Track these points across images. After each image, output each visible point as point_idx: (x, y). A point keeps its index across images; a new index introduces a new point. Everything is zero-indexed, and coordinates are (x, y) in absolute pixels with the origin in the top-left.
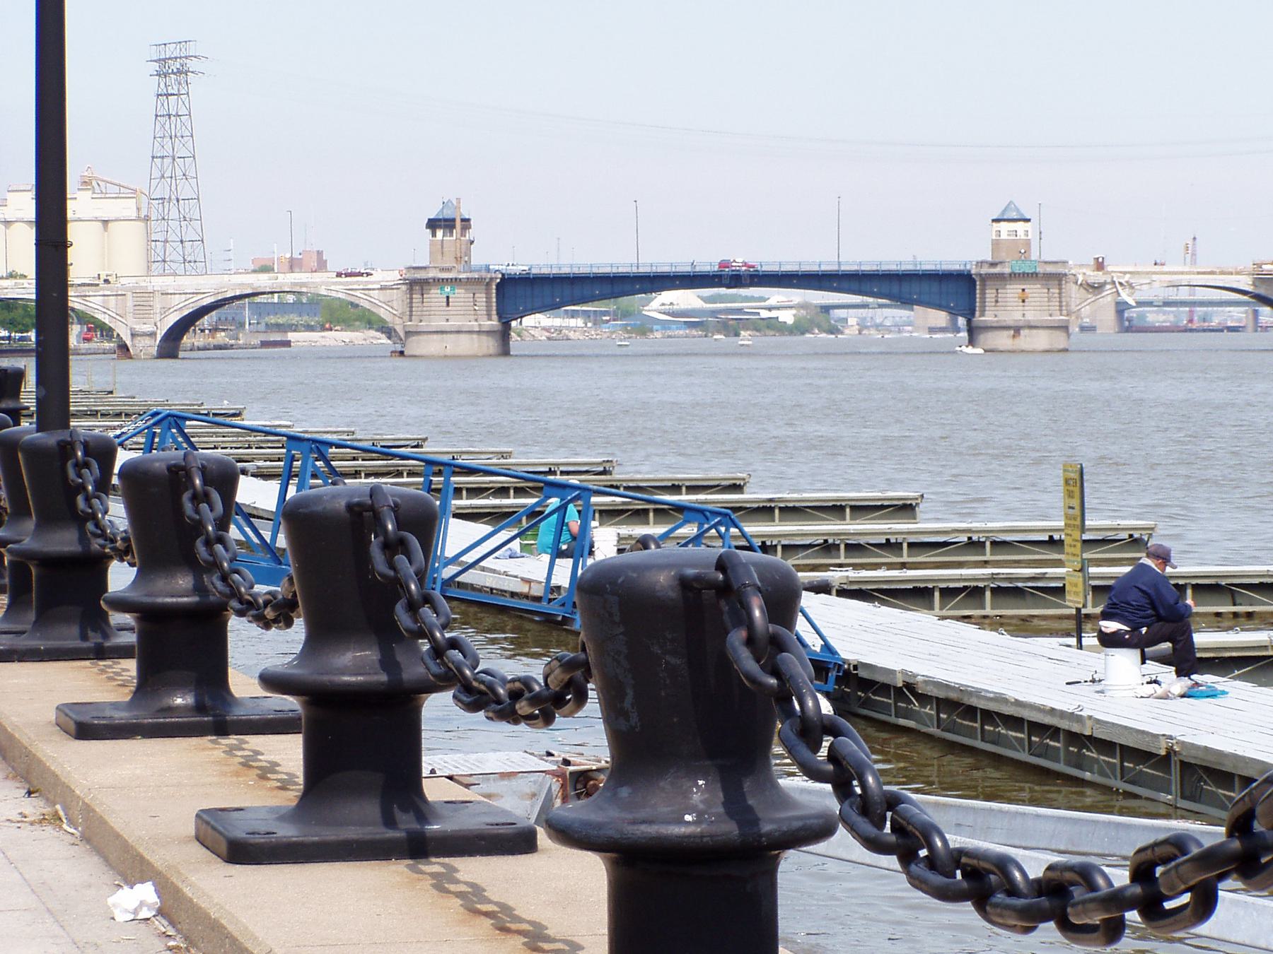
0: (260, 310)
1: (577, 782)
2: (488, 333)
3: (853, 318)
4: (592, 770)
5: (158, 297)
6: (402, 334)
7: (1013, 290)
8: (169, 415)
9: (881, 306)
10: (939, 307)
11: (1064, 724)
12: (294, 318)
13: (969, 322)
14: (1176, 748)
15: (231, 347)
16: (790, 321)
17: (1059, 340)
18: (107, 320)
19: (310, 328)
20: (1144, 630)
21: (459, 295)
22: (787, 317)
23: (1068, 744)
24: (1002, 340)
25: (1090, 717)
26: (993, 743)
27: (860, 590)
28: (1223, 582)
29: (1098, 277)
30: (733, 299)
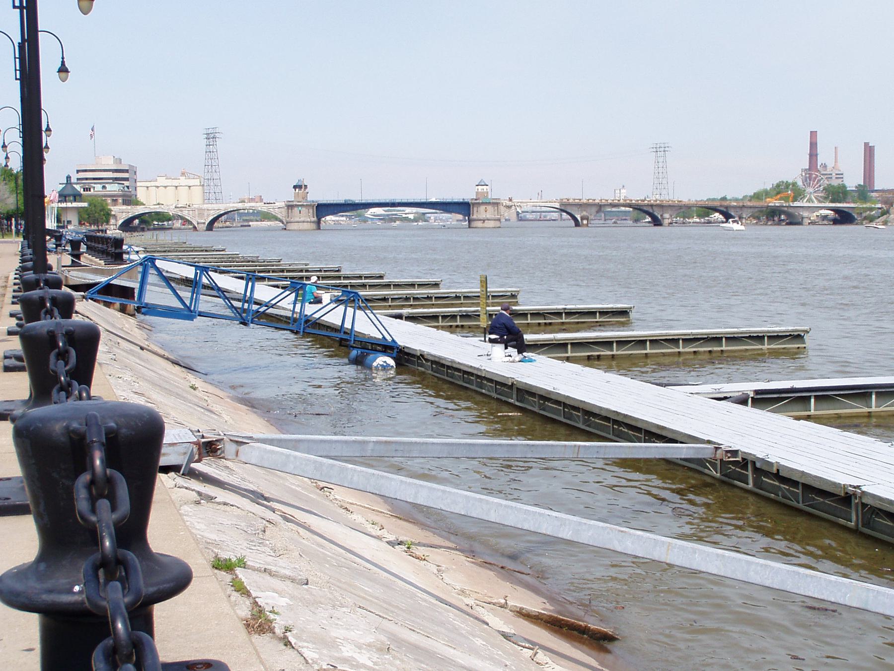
0: (241, 215)
1: (207, 446)
2: (313, 222)
3: (432, 217)
4: (213, 441)
5: (206, 211)
6: (285, 223)
7: (482, 208)
8: (150, 258)
9: (441, 213)
10: (459, 213)
11: (475, 372)
12: (252, 217)
13: (468, 218)
14: (515, 383)
15: (231, 227)
16: (412, 218)
17: (497, 224)
18: (189, 219)
19: (257, 221)
20: (505, 337)
21: (304, 210)
22: (411, 217)
23: (476, 379)
24: (479, 224)
25: (484, 370)
26: (452, 378)
27: (413, 317)
28: (541, 312)
29: (510, 203)
30: (394, 211)
